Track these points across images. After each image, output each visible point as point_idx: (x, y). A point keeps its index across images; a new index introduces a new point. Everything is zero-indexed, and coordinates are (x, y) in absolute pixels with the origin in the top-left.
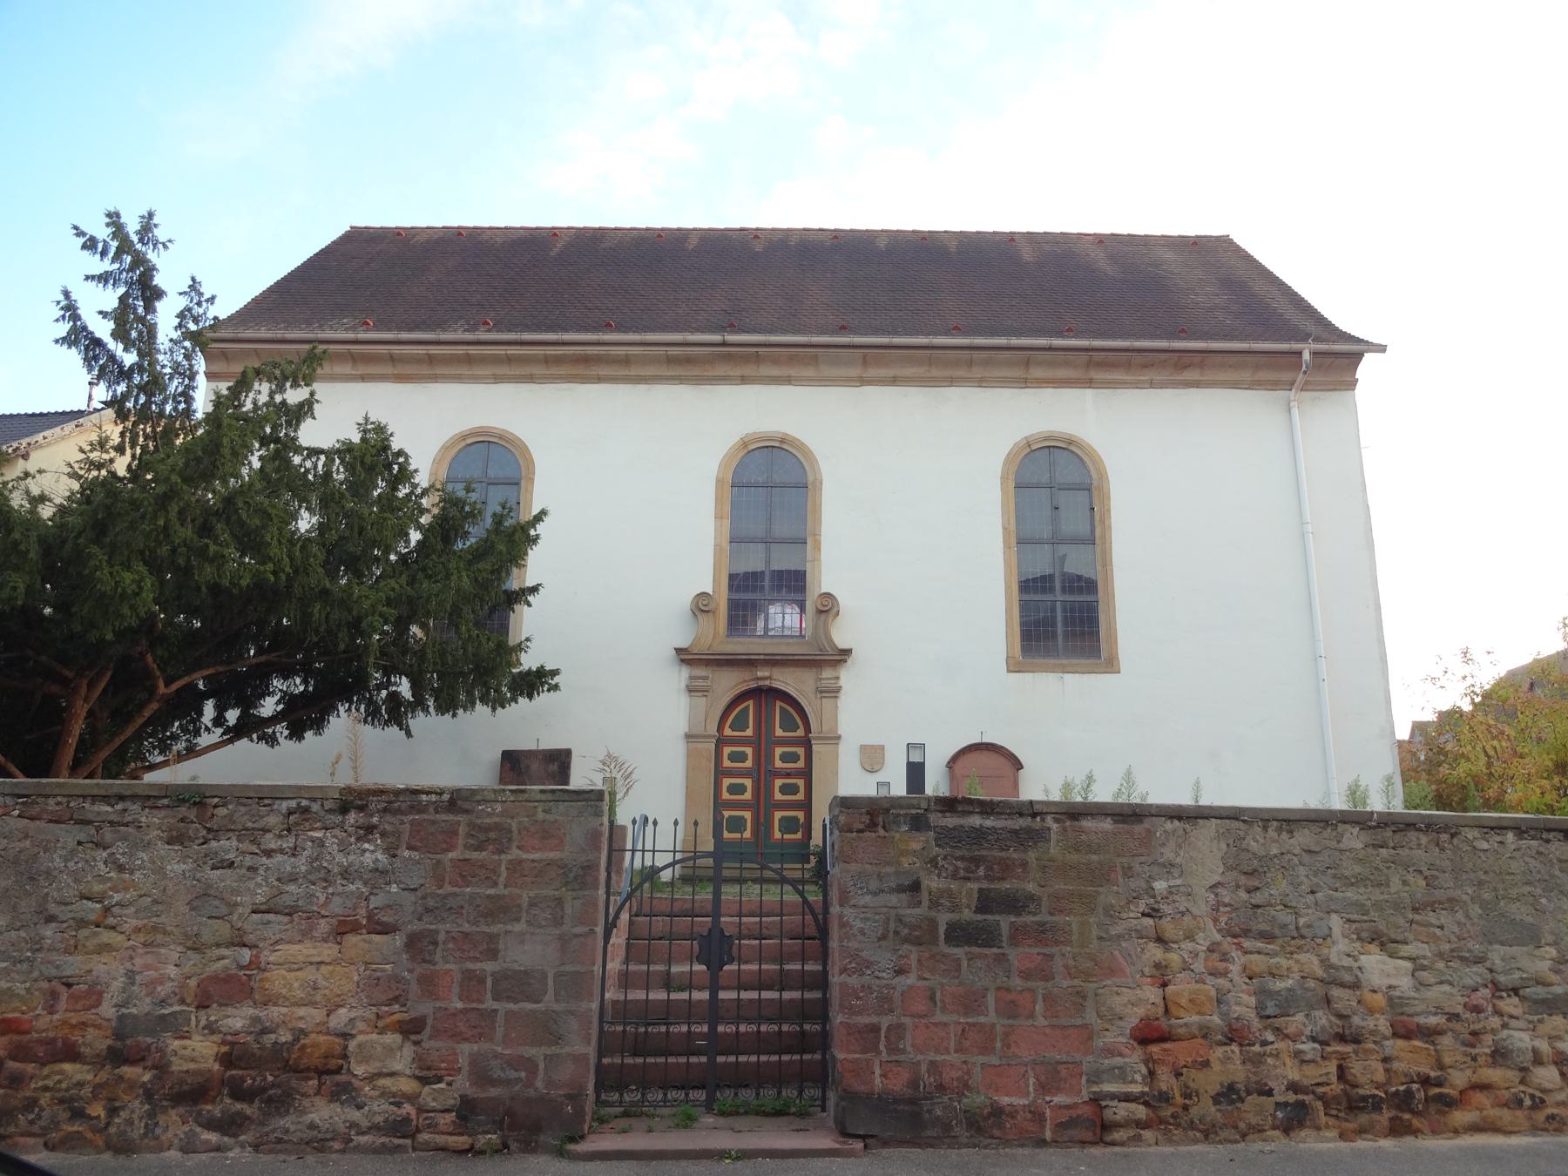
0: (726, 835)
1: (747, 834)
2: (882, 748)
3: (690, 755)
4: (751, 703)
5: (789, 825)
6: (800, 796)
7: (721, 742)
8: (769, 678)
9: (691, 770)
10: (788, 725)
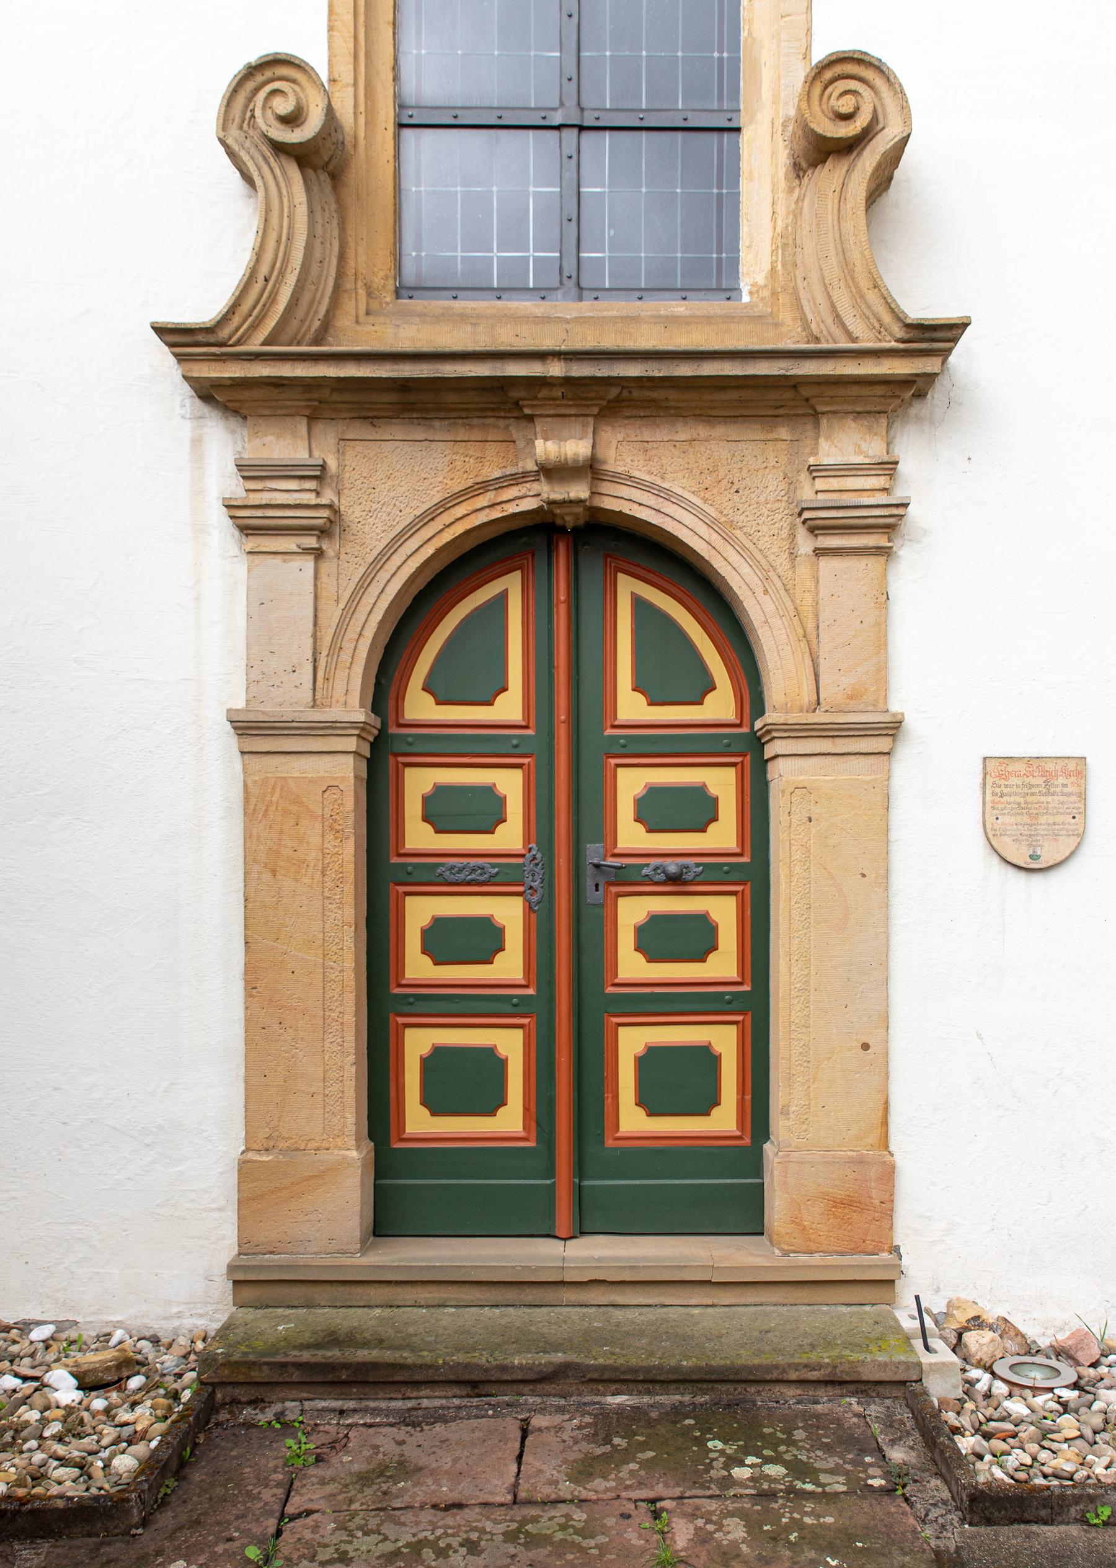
0: (419, 1121)
1: (509, 1119)
2: (1076, 768)
3: (259, 807)
4: (512, 584)
5: (679, 1081)
6: (723, 965)
7: (384, 754)
8: (591, 469)
9: (265, 863)
10: (670, 673)
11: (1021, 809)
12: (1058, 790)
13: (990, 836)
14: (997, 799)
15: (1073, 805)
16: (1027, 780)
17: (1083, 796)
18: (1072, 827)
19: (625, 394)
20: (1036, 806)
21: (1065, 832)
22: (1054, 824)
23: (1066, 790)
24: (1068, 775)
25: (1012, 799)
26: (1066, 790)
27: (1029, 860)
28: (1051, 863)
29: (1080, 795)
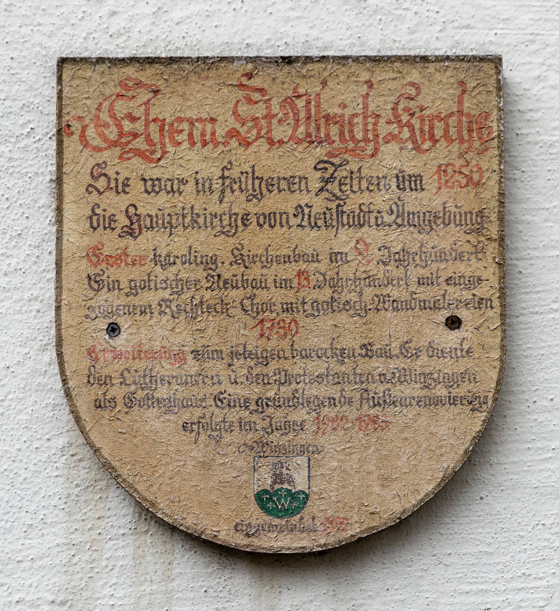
11: (220, 286)
12: (381, 200)
13: (84, 406)
14: (112, 243)
15: (448, 269)
16: (243, 159)
17: (495, 230)
18: (449, 367)
19: (475, 169)
20: (289, 271)
21: (413, 390)
22: (368, 350)
23: (413, 201)
24: (423, 137)
25: (179, 244)
26: (413, 201)
27: (255, 515)
28: (355, 530)
29: (476, 223)
